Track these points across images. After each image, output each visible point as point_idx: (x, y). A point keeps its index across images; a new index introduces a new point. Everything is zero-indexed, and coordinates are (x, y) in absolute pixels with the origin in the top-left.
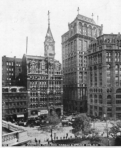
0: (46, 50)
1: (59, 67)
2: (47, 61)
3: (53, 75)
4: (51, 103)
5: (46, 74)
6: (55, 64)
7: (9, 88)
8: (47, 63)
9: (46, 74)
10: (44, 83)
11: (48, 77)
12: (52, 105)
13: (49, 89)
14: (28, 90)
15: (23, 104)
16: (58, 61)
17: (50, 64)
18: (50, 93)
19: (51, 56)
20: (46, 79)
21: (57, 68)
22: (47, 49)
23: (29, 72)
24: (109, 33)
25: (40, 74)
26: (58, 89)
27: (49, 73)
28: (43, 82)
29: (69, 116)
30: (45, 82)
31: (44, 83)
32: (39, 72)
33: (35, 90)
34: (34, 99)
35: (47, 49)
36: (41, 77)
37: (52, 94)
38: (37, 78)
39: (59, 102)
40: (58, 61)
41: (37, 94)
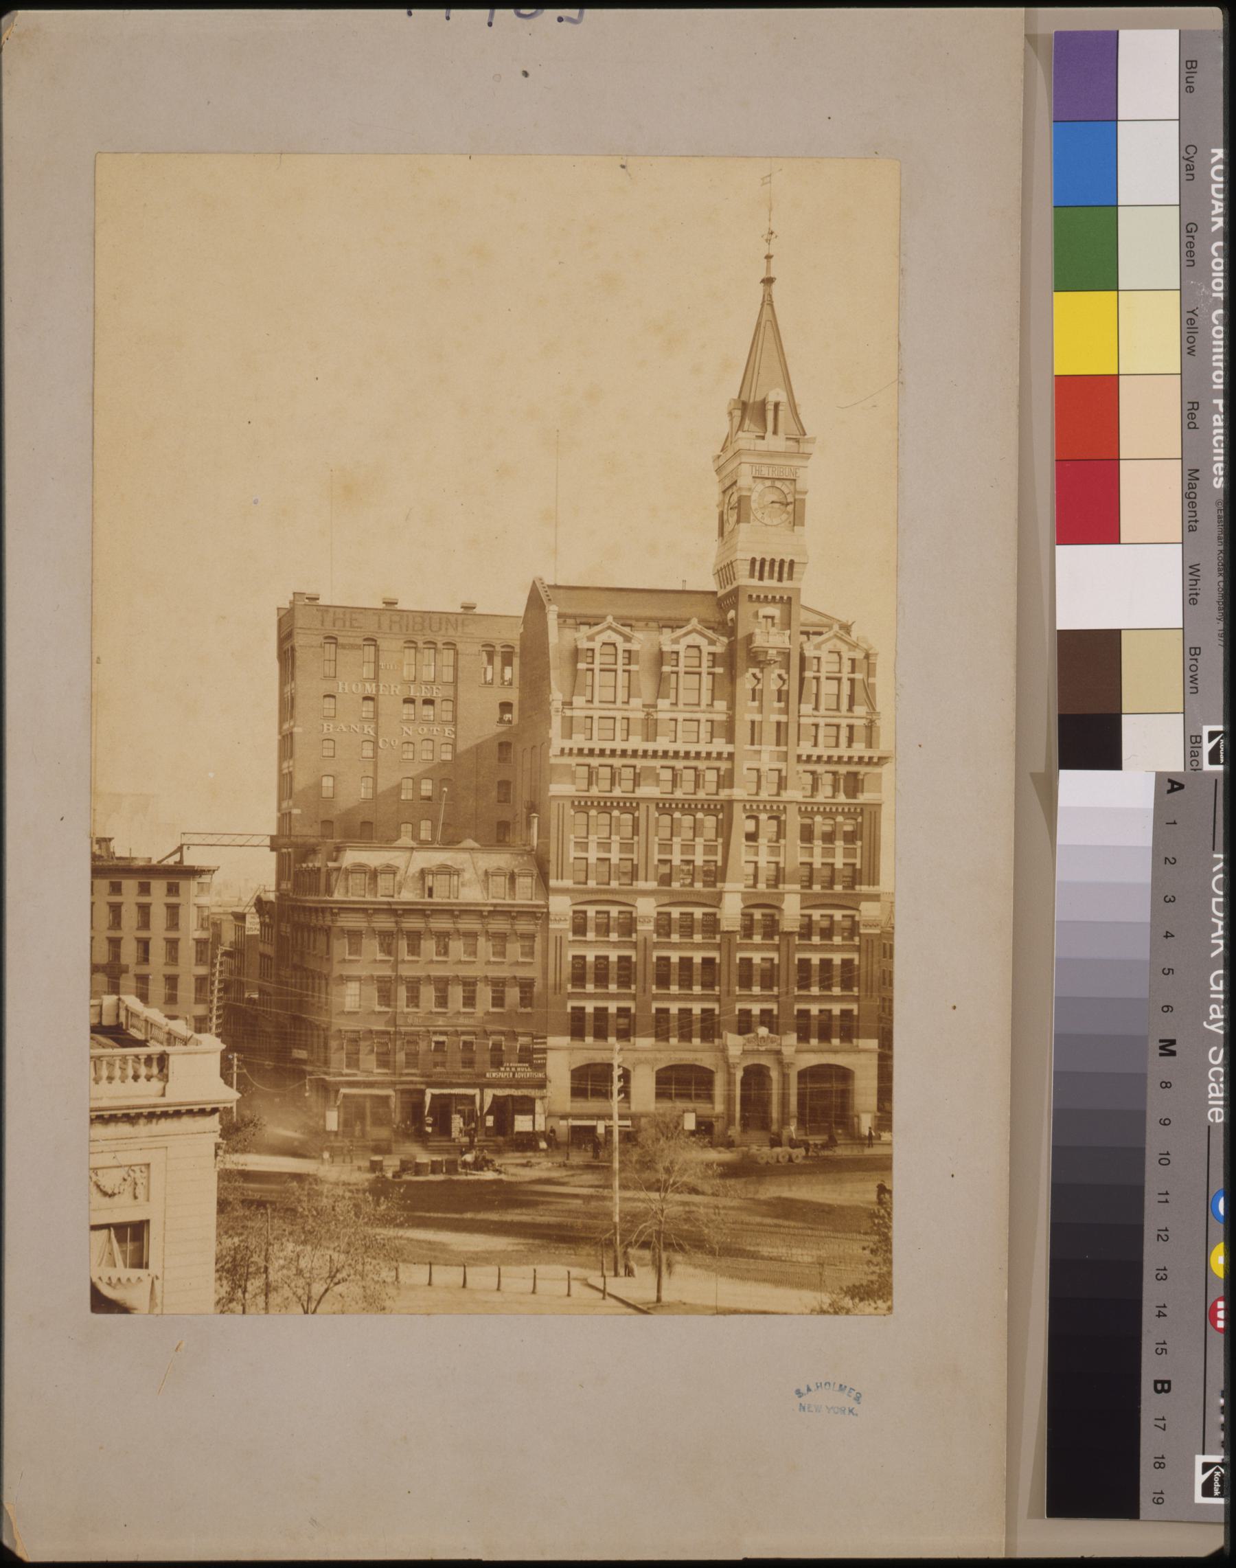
0: (728, 528)
1: (845, 675)
2: (728, 629)
3: (784, 757)
4: (756, 1009)
5: (720, 745)
6: (809, 652)
7: (402, 865)
8: (731, 648)
9: (720, 745)
10: (696, 829)
11: (731, 772)
12: (763, 1031)
13: (797, 887)
14: (553, 883)
15: (428, 994)
16: (846, 628)
17: (757, 659)
18: (747, 916)
19: (767, 582)
20: (719, 786)
21: (828, 688)
22: (738, 521)
23: (568, 733)
24: (797, 401)
25: (662, 744)
26: (831, 883)
27: (742, 731)
28: (688, 821)
29: (789, 1125)
30: (710, 822)
31: (696, 829)
32: (651, 728)
33: (614, 884)
34: (826, 964)
35: (738, 521)
36: (666, 775)
37: (771, 927)
38: (636, 781)
39: (836, 1009)
40: (846, 628)
41: (628, 925)
